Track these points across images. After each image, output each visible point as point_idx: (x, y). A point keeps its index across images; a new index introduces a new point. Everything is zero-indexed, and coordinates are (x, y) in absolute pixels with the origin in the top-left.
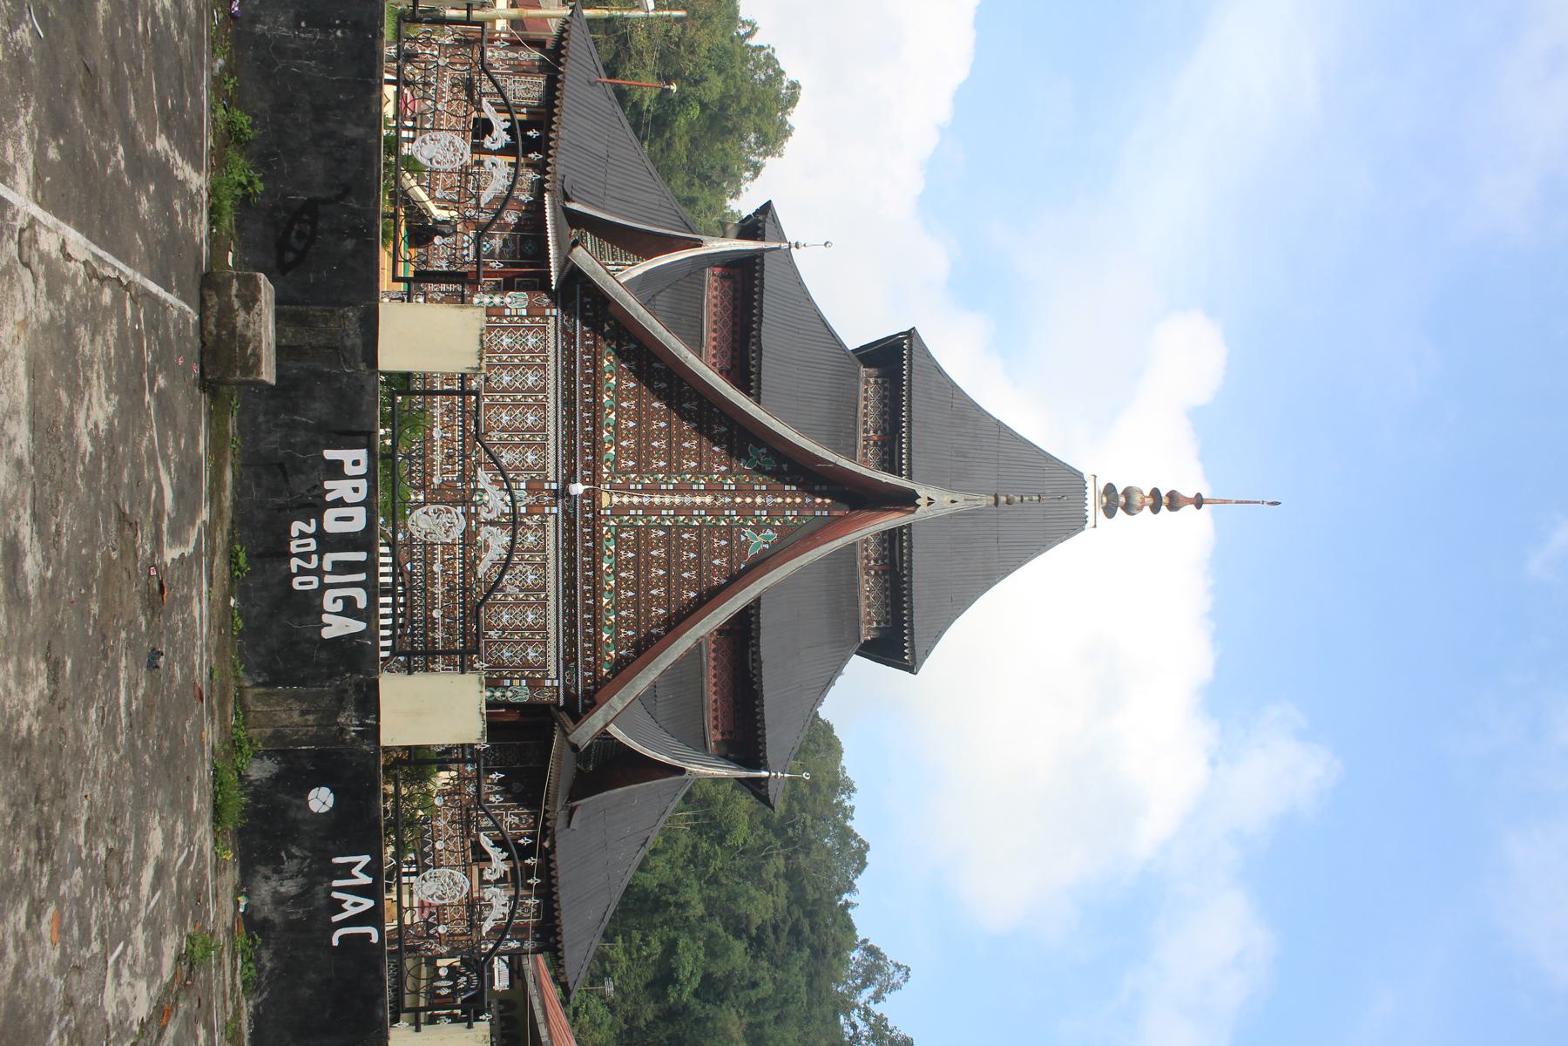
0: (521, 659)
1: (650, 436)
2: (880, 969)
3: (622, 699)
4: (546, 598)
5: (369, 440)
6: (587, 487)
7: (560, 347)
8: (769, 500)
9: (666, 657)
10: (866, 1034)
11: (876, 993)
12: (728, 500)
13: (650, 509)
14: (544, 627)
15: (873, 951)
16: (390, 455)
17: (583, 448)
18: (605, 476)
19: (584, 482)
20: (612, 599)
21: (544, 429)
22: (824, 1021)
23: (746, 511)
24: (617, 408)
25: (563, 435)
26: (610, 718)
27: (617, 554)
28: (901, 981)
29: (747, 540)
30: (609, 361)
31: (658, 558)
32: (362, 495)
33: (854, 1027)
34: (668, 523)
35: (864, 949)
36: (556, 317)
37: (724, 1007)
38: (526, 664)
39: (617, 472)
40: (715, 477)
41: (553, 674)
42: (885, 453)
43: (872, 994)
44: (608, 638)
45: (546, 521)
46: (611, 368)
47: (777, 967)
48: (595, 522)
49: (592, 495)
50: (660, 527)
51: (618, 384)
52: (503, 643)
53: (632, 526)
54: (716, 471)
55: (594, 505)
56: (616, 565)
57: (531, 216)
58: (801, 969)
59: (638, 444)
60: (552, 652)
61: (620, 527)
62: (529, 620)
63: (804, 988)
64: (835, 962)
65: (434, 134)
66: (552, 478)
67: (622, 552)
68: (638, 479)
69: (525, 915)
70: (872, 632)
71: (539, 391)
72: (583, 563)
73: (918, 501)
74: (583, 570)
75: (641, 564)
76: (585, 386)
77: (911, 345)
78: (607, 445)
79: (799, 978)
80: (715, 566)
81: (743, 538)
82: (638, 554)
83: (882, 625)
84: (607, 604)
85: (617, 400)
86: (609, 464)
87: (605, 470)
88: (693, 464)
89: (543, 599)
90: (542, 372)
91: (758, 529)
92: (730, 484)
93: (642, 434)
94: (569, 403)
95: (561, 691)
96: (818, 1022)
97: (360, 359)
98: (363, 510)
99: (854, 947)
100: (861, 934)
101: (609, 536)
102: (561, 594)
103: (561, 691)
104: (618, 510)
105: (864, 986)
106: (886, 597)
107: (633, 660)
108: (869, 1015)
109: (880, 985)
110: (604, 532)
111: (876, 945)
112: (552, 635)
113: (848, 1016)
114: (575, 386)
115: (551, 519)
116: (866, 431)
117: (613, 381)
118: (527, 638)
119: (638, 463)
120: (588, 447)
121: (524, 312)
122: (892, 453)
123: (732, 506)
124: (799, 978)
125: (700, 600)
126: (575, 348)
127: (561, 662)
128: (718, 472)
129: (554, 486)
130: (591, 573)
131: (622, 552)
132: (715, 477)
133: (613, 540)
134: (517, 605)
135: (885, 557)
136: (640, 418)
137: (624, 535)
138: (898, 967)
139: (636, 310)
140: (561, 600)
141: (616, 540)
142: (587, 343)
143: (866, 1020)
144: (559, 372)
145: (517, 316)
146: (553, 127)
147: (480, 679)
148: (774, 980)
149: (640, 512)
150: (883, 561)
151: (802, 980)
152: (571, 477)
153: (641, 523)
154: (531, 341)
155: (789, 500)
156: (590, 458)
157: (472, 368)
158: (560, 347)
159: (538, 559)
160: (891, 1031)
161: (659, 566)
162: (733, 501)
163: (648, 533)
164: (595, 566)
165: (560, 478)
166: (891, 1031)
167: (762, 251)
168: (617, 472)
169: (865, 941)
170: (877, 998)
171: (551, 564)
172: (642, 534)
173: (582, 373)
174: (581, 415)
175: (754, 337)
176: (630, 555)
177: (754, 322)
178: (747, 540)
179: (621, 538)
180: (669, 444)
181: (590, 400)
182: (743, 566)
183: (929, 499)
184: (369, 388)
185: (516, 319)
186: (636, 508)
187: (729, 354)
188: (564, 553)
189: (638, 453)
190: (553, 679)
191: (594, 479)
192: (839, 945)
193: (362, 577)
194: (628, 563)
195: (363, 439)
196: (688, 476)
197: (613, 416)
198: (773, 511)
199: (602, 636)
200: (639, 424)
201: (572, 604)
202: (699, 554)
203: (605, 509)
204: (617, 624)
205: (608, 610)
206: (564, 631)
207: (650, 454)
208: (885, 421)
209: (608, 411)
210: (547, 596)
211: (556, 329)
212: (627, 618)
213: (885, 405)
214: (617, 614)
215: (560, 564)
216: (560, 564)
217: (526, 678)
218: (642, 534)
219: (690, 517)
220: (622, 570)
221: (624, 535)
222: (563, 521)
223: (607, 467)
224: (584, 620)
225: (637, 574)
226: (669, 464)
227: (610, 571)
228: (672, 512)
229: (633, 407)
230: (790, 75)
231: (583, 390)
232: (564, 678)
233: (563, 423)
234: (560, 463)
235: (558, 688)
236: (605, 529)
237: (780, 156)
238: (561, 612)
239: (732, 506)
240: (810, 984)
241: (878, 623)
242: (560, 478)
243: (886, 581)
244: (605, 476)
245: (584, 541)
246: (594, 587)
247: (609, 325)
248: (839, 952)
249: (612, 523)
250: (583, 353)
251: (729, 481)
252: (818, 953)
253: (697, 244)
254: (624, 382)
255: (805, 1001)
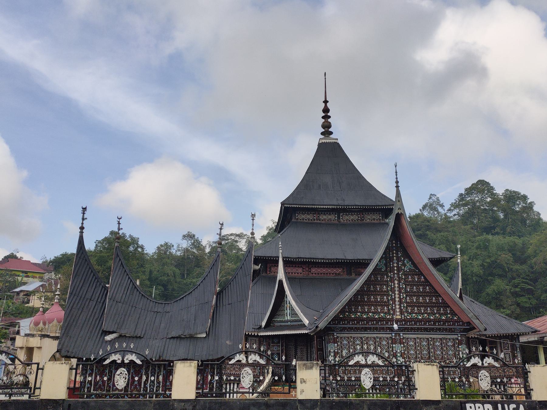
0: (452, 347)
1: (376, 301)
2: (431, 205)
3: (469, 313)
4: (431, 338)
5: (463, 403)
6: (394, 323)
7: (347, 332)
8: (395, 261)
9: (455, 298)
10: (458, 211)
11: (440, 206)
12: (396, 275)
13: (400, 301)
14: (441, 339)
15: (424, 207)
16: (466, 396)
17: (381, 324)
18: (390, 317)
19: (393, 324)
20: (431, 315)
21: (375, 338)
22: (454, 226)
23: (399, 269)
24: (368, 313)
25: (383, 331)
26: (475, 317)
27: (416, 313)
28: (436, 197)
29: (409, 269)
30: (352, 315)
31: (416, 299)
32: (480, 405)
33: (455, 215)
34: (405, 296)
35: (423, 210)
36: (337, 333)
37: (450, 264)
38: (454, 345)
39: (389, 313)
40: (388, 279)
41: (456, 336)
42: (322, 214)
43: (441, 208)
44: (444, 317)
45: (405, 337)
46: (355, 314)
47: (434, 244)
48: (406, 321)
49: (397, 321)
50: (406, 298)
51: (360, 312)
52: (447, 353)
53: (406, 308)
54: (386, 279)
55: (400, 321)
56: (419, 314)
57: (265, 340)
58: (435, 235)
59: (379, 305)
60: (449, 337)
61: (407, 312)
62: (439, 344)
63: (442, 234)
64: (431, 222)
65: (362, 381)
66: (391, 335)
67: (415, 312)
68: (391, 306)
69: (508, 346)
70: (383, 219)
71: (362, 340)
72: (419, 325)
73: (400, 213)
74: (422, 325)
75: (419, 305)
76: (361, 324)
77: (286, 204)
78: (380, 316)
79: (438, 235)
80: (418, 280)
81: (408, 270)
82: (416, 306)
83: (381, 215)
84: (433, 317)
85: (365, 313)
86: (386, 316)
87: (388, 317)
88: (385, 287)
89: (431, 339)
90: (355, 339)
91: (404, 265)
92: (391, 275)
93: (376, 304)
94: (366, 329)
95: (462, 334)
96: (455, 229)
97: (438, 406)
98: (476, 405)
99: (423, 215)
100: (418, 212)
101: (410, 316)
102: (429, 333)
103: (462, 334)
104: (401, 313)
105: (437, 211)
106: (371, 214)
107: (451, 308)
108: (451, 210)
109: (437, 205)
110: (409, 318)
111: (422, 206)
112: (443, 336)
113: (450, 217)
114: (360, 327)
115: (404, 336)
116: (314, 220)
117: (359, 314)
118: (445, 345)
119: (385, 305)
120: (381, 323)
121: (336, 345)
122: (322, 211)
123: (398, 274)
124: (438, 235)
125: (429, 285)
126: (348, 327)
127: (452, 333)
128: (387, 279)
129: (393, 335)
130: (423, 322)
131: (415, 312)
132: (388, 279)
133: (412, 315)
134: (434, 348)
135: (357, 214)
136: (371, 305)
137: (410, 311)
138: (430, 198)
139: (340, 306)
140: (431, 333)
141: (412, 314)
142: (346, 323)
143: (453, 210)
144: (355, 332)
145: (337, 347)
146: (250, 334)
147: (533, 366)
148: (439, 244)
149: (402, 305)
150: (358, 215)
151: (439, 235)
152: (392, 329)
153: (405, 305)
154: (345, 342)
155: (395, 255)
156: (384, 322)
157: (437, 368)
158: (347, 332)
159: (418, 341)
160: (456, 201)
161: (419, 299)
162: (396, 273)
163: (408, 303)
164: (420, 321)
165: (391, 332)
166: (456, 201)
167: (283, 258)
168: (389, 313)
169: (420, 210)
170: (442, 206)
171: (420, 336)
172: (409, 305)
173: (356, 324)
174: (370, 325)
175: (293, 260)
176: (416, 309)
177: (288, 260)
178: (409, 269)
179: (411, 312)
180: (379, 295)
181: (365, 322)
182: (417, 271)
183: (399, 209)
184: (447, 403)
185: (338, 348)
186: (401, 306)
187: (297, 268)
188: (416, 332)
189: (382, 305)
190: (458, 336)
191: (391, 320)
192: (425, 220)
193: (506, 406)
194: (419, 309)
195: (463, 405)
196: (389, 289)
197: (371, 314)
198: (398, 260)
199: (444, 319)
200: (372, 305)
201: (432, 329)
202: (414, 285)
203: (402, 317)
204: (439, 314)
205: (435, 317)
206: (442, 332)
207: (382, 302)
208: (311, 213)
209: (369, 316)
210: (430, 338)
211: (341, 333)
212: (437, 310)
213: (305, 213)
214: (436, 314)
215: (419, 333)
216: (419, 333)
217: (459, 345)
218: (409, 305)
219: (403, 288)
220: (421, 312)
221: (410, 311)
222: (405, 331)
223: (387, 316)
224: (439, 325)
225: (422, 306)
226: (385, 295)
227: (422, 316)
228: (401, 294)
229: (367, 307)
230: (107, 234)
231: (362, 324)
232: (457, 332)
233: (372, 331)
234: (386, 332)
235: (461, 335)
236: (408, 317)
237: (138, 239)
238: (435, 333)
239: (398, 274)
240: (440, 232)
241: (380, 217)
242: (391, 332)
243: (365, 214)
244: (390, 317)
245: (412, 325)
246: (427, 321)
247: (340, 315)
248: (428, 220)
249: (406, 315)
250: (349, 324)
251: (390, 275)
252: (428, 228)
253: (281, 282)
254: (346, 310)
255: (447, 233)
